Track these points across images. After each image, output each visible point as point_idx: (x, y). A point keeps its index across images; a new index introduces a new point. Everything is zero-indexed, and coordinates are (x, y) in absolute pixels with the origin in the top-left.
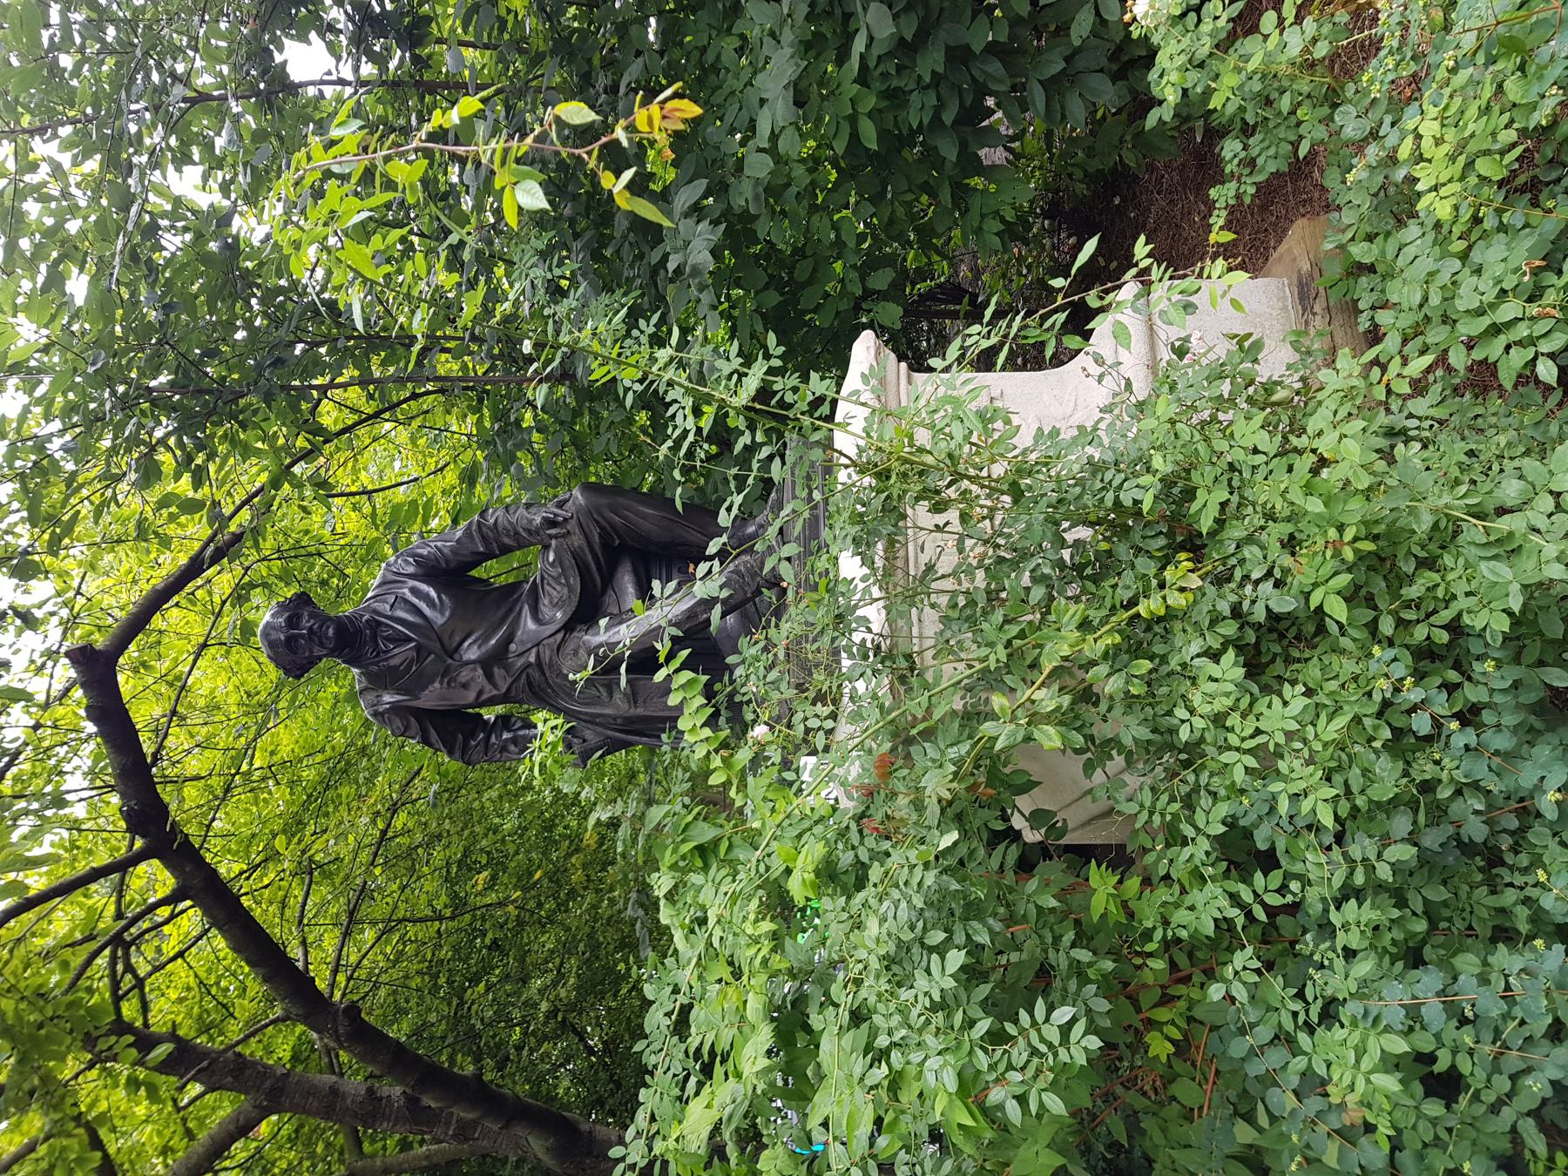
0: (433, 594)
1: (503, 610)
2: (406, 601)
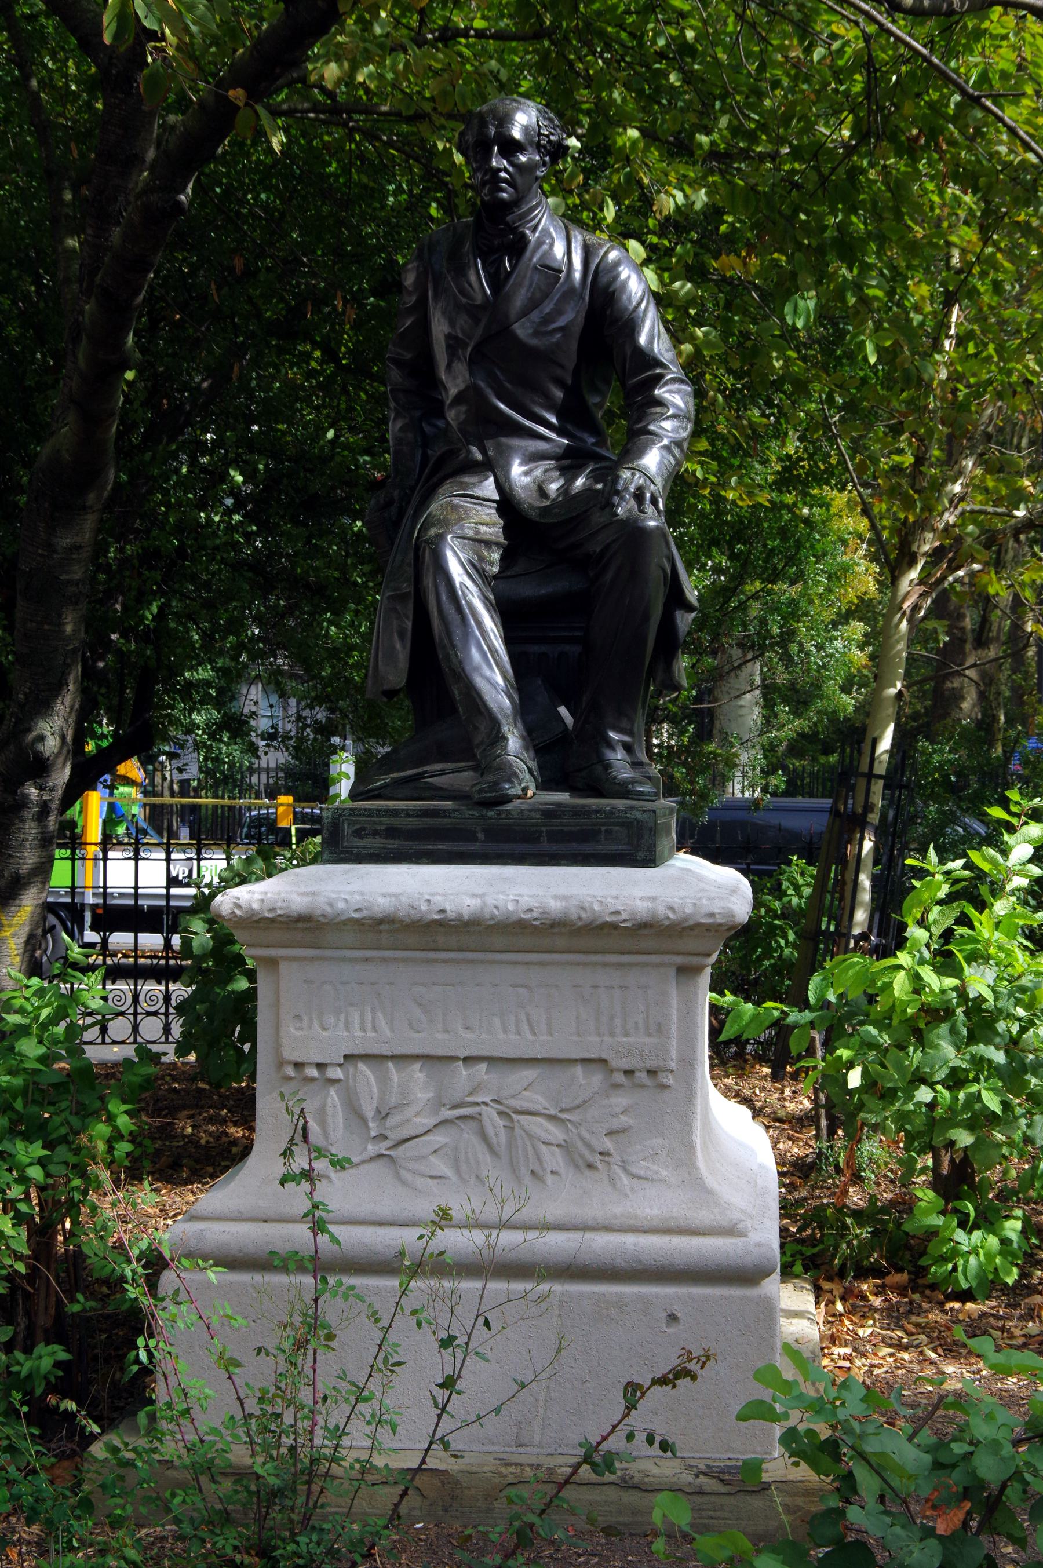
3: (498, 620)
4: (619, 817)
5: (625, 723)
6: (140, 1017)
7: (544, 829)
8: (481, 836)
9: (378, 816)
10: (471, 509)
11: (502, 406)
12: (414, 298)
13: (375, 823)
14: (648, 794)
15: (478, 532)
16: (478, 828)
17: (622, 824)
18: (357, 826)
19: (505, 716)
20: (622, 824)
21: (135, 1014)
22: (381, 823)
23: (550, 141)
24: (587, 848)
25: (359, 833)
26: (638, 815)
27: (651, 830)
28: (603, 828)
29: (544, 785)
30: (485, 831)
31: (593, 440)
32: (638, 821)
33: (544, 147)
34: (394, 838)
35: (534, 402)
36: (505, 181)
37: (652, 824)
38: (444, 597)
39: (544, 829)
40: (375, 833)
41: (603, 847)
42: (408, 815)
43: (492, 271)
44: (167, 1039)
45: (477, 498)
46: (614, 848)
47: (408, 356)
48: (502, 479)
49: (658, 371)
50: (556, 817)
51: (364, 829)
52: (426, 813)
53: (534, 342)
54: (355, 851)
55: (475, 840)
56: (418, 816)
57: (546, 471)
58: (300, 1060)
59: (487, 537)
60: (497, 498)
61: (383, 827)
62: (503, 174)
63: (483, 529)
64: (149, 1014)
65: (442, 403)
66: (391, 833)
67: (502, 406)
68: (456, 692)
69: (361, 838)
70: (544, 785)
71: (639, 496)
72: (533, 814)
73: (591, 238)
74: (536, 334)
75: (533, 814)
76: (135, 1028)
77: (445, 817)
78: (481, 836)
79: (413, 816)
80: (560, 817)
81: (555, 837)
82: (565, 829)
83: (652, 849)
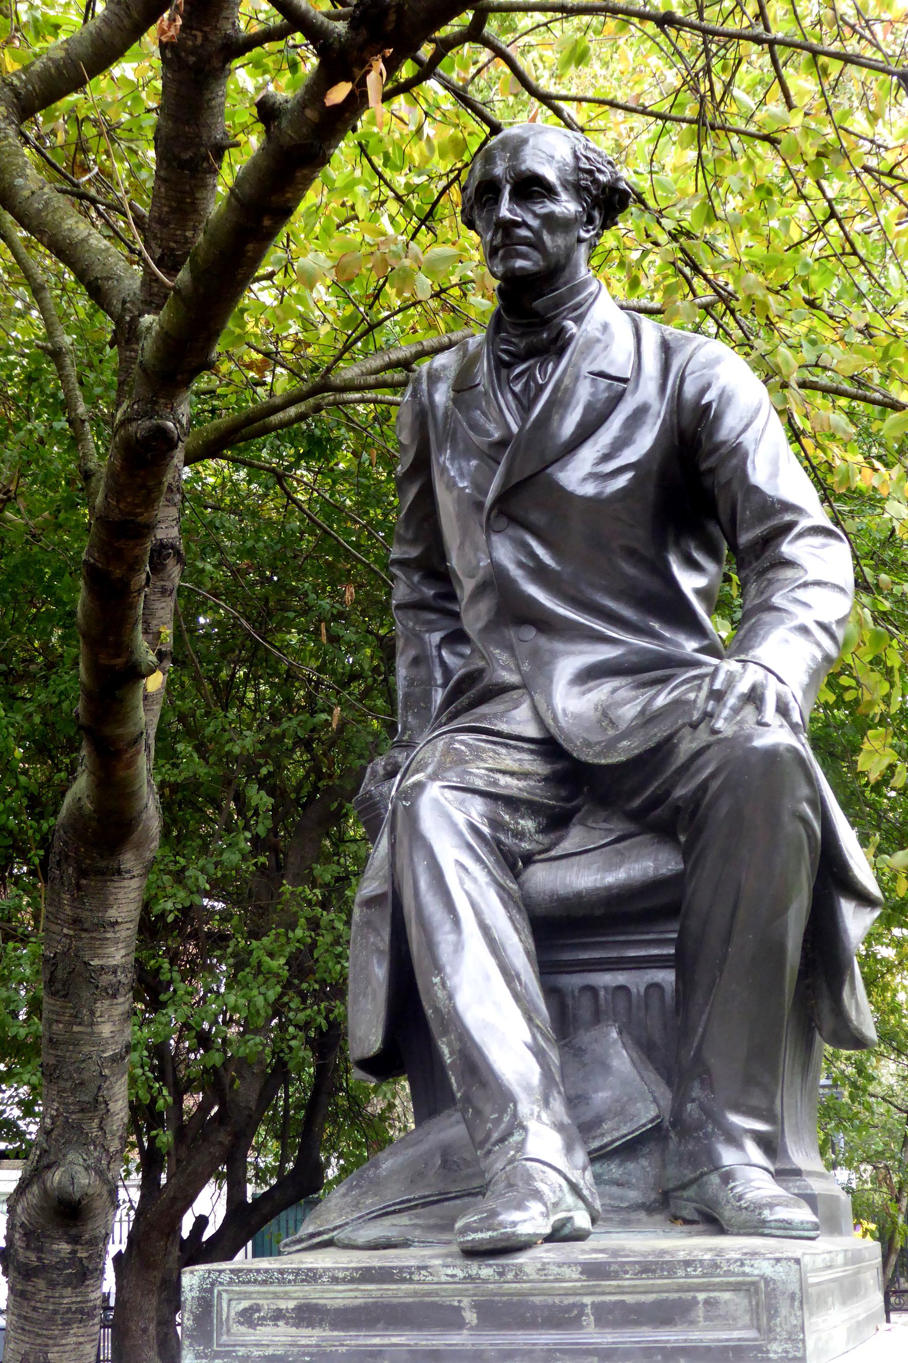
0: (631, 455)
1: (627, 612)
2: (616, 399)
3: (527, 931)
4: (728, 1273)
5: (757, 1100)
7: (587, 1300)
8: (470, 1317)
9: (282, 1282)
10: (484, 750)
13: (276, 1296)
14: (802, 1226)
15: (495, 783)
16: (466, 1302)
17: (736, 1288)
18: (245, 1304)
19: (528, 1089)
20: (736, 1288)
22: (287, 1296)
23: (595, 181)
25: (248, 1317)
26: (764, 1268)
27: (792, 1297)
28: (701, 1296)
30: (478, 1307)
32: (767, 1281)
33: (586, 189)
34: (311, 1324)
36: (525, 242)
37: (794, 1287)
38: (423, 884)
39: (587, 1300)
40: (278, 1316)
42: (335, 1280)
45: (498, 734)
46: (724, 1335)
48: (542, 707)
50: (607, 1276)
51: (258, 1309)
52: (367, 1275)
54: (241, 1351)
56: (352, 1281)
57: (614, 691)
59: (514, 792)
61: (291, 1304)
62: (524, 232)
63: (504, 780)
68: (446, 1050)
69: (252, 1325)
71: (754, 697)
72: (567, 1272)
73: (670, 330)
75: (567, 1272)
77: (403, 1281)
78: (470, 1317)
79: (344, 1281)
80: (616, 1276)
82: (629, 1299)
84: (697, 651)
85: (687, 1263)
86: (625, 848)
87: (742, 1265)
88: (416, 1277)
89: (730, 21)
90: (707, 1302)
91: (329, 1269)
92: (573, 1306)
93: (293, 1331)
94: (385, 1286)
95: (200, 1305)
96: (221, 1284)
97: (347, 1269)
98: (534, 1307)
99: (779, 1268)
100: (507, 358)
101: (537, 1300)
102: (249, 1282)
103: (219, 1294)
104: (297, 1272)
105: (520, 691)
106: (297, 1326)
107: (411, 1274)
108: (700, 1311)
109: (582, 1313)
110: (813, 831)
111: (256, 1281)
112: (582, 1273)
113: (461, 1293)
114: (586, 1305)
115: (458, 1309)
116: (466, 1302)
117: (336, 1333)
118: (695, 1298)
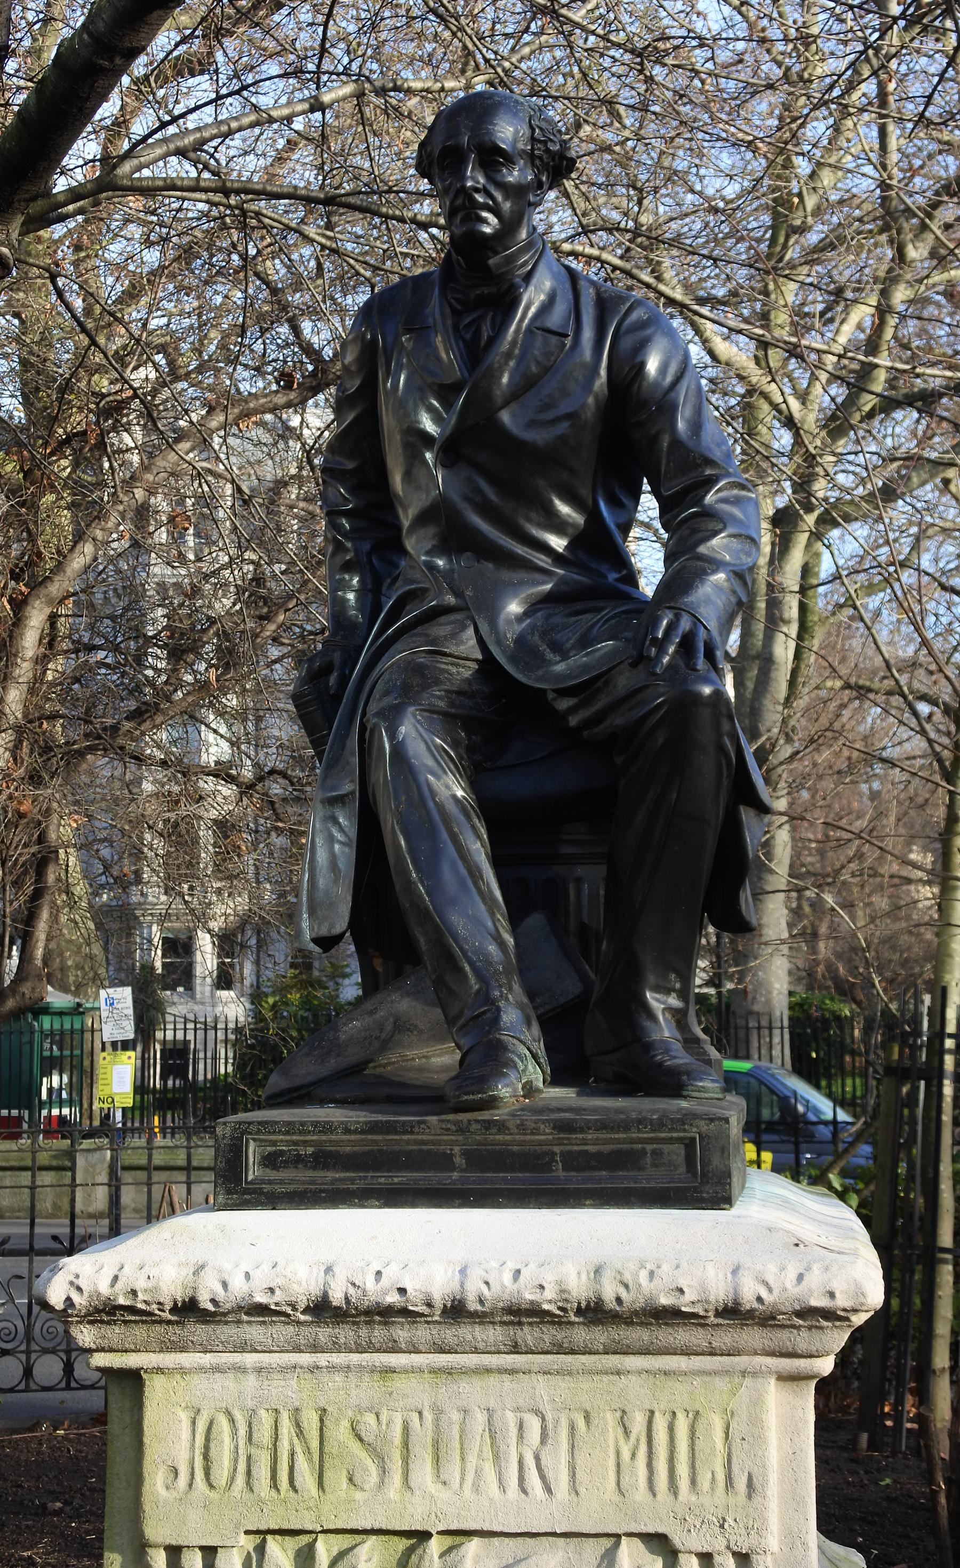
6: (34, 1356)
7: (557, 1149)
8: (459, 1160)
11: (403, 843)
12: (357, 382)
16: (457, 1149)
21: (28, 1352)
23: (547, 151)
24: (625, 1179)
28: (649, 1148)
29: (556, 1079)
30: (466, 1154)
31: (616, 575)
34: (326, 1167)
35: (529, 520)
40: (298, 1161)
41: (651, 1178)
43: (468, 336)
44: (68, 1383)
45: (450, 655)
47: (350, 465)
49: (708, 472)
53: (530, 436)
55: (452, 1168)
56: (363, 1132)
58: (174, 1543)
60: (480, 657)
61: (310, 1150)
64: (45, 1351)
65: (398, 528)
66: (323, 1159)
67: (403, 843)
68: (422, 940)
70: (556, 1079)
74: (532, 424)
76: (28, 1372)
77: (405, 1132)
78: (459, 1160)
79: (355, 1132)
80: (582, 1131)
81: (573, 1161)
82: (590, 1148)
83: (725, 1178)
84: (617, 580)
85: (640, 1122)
86: (750, 832)
87: (684, 1124)
88: (416, 1130)
89: (905, 736)
90: (654, 1152)
91: (342, 1123)
92: (545, 1154)
93: (311, 1174)
94: (390, 1137)
95: (231, 1151)
96: (250, 1133)
97: (358, 1122)
98: (512, 1154)
99: (712, 1126)
100: (459, 307)
101: (515, 1148)
102: (274, 1132)
103: (247, 1140)
104: (316, 1124)
105: (458, 616)
106: (314, 1168)
107: (412, 1127)
108: (648, 1159)
109: (553, 1160)
110: (731, 759)
111: (280, 1131)
112: (554, 1128)
113: (456, 1143)
114: (555, 1154)
115: (451, 1156)
116: (457, 1149)
117: (348, 1174)
118: (644, 1149)
